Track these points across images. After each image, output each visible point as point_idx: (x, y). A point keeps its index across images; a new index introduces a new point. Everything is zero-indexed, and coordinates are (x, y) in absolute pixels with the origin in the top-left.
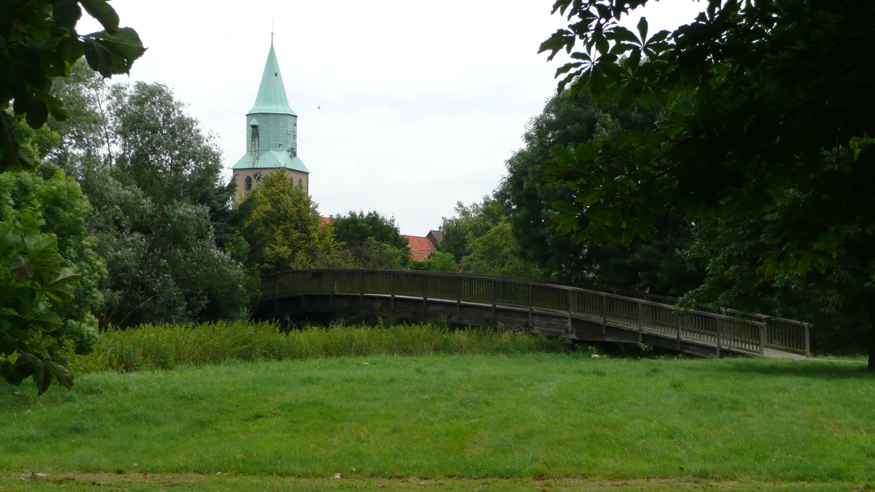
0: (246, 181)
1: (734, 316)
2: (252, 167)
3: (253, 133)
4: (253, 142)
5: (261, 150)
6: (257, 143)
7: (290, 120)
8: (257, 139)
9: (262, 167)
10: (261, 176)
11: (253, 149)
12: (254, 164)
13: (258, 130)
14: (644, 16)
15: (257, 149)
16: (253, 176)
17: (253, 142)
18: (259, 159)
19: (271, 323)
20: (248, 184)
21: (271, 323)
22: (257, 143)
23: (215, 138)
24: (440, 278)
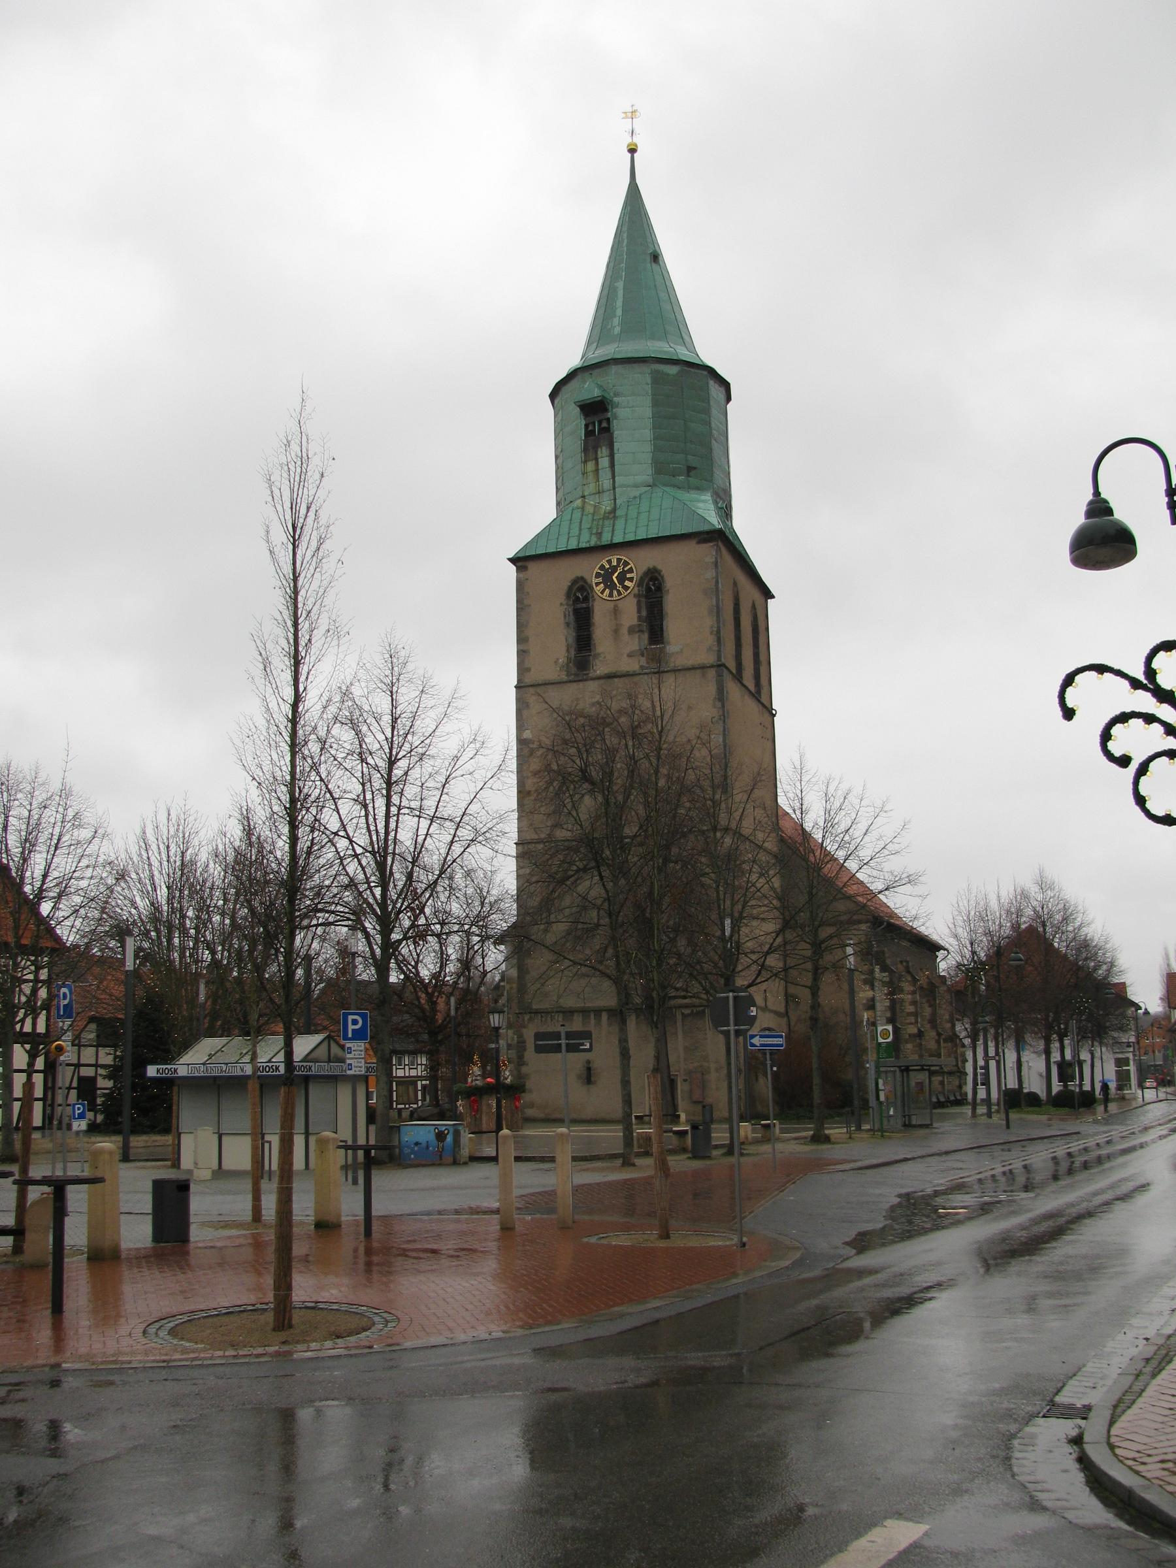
0: (568, 595)
1: (120, 1113)
2: (593, 544)
3: (589, 433)
4: (591, 466)
5: (622, 486)
6: (604, 462)
7: (715, 391)
8: (603, 452)
9: (630, 537)
10: (631, 571)
11: (591, 488)
12: (599, 535)
13: (608, 420)
14: (1075, 718)
15: (606, 483)
16: (598, 575)
17: (591, 466)
18: (615, 517)
19: (1086, 935)
20: (576, 612)
21: (1086, 935)
22: (604, 462)
23: (633, 114)
24: (60, 1122)
